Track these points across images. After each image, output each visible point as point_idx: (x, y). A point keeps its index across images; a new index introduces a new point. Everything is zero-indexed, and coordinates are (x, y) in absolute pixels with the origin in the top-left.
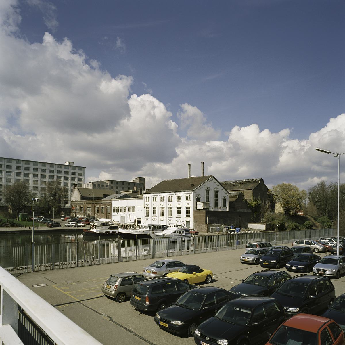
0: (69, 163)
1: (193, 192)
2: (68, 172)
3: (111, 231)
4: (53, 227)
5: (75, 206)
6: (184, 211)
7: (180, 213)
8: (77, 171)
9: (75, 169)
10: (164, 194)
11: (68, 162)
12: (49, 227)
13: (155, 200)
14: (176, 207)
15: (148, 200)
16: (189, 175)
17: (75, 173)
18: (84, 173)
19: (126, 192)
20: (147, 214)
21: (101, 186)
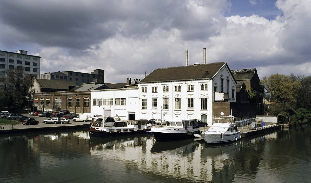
0: (22, 51)
1: (212, 80)
2: (21, 61)
3: (116, 129)
4: (29, 124)
5: (39, 98)
6: (197, 103)
7: (156, 106)
8: (31, 61)
10: (169, 83)
11: (20, 50)
12: (24, 125)
14: (186, 98)
15: (144, 90)
16: (187, 63)
17: (29, 62)
18: (39, 63)
19: (88, 84)
20: (144, 106)
21: (59, 77)
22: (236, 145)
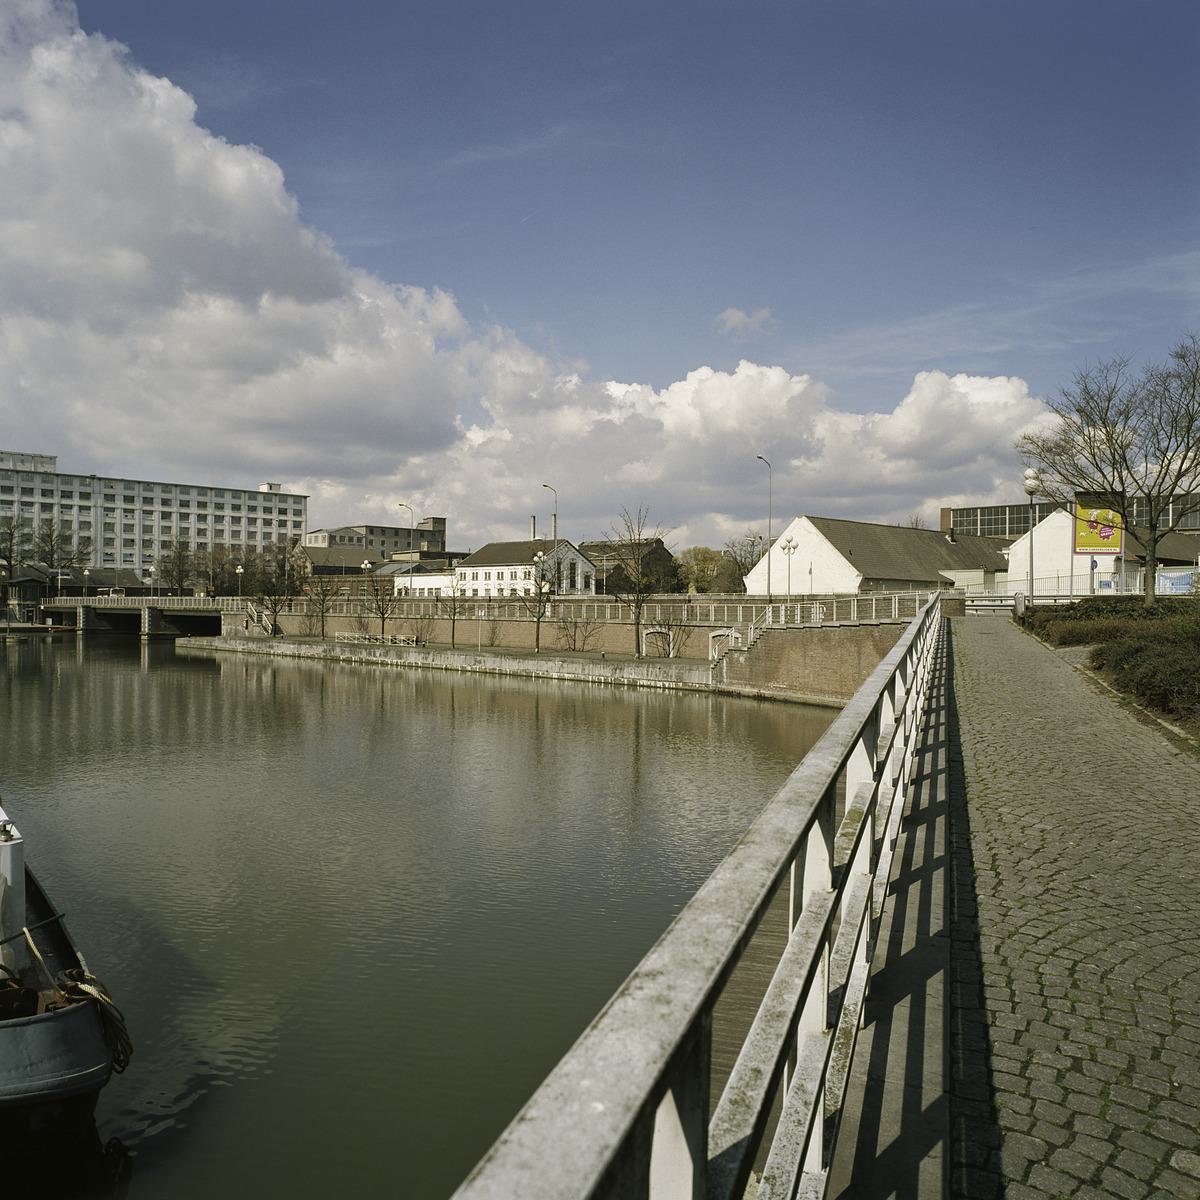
2: (271, 508)
8: (290, 505)
9: (188, 494)
13: (475, 577)
18: (306, 510)
21: (347, 538)
22: (135, 1153)
